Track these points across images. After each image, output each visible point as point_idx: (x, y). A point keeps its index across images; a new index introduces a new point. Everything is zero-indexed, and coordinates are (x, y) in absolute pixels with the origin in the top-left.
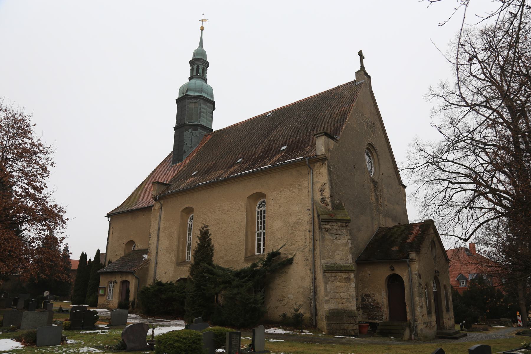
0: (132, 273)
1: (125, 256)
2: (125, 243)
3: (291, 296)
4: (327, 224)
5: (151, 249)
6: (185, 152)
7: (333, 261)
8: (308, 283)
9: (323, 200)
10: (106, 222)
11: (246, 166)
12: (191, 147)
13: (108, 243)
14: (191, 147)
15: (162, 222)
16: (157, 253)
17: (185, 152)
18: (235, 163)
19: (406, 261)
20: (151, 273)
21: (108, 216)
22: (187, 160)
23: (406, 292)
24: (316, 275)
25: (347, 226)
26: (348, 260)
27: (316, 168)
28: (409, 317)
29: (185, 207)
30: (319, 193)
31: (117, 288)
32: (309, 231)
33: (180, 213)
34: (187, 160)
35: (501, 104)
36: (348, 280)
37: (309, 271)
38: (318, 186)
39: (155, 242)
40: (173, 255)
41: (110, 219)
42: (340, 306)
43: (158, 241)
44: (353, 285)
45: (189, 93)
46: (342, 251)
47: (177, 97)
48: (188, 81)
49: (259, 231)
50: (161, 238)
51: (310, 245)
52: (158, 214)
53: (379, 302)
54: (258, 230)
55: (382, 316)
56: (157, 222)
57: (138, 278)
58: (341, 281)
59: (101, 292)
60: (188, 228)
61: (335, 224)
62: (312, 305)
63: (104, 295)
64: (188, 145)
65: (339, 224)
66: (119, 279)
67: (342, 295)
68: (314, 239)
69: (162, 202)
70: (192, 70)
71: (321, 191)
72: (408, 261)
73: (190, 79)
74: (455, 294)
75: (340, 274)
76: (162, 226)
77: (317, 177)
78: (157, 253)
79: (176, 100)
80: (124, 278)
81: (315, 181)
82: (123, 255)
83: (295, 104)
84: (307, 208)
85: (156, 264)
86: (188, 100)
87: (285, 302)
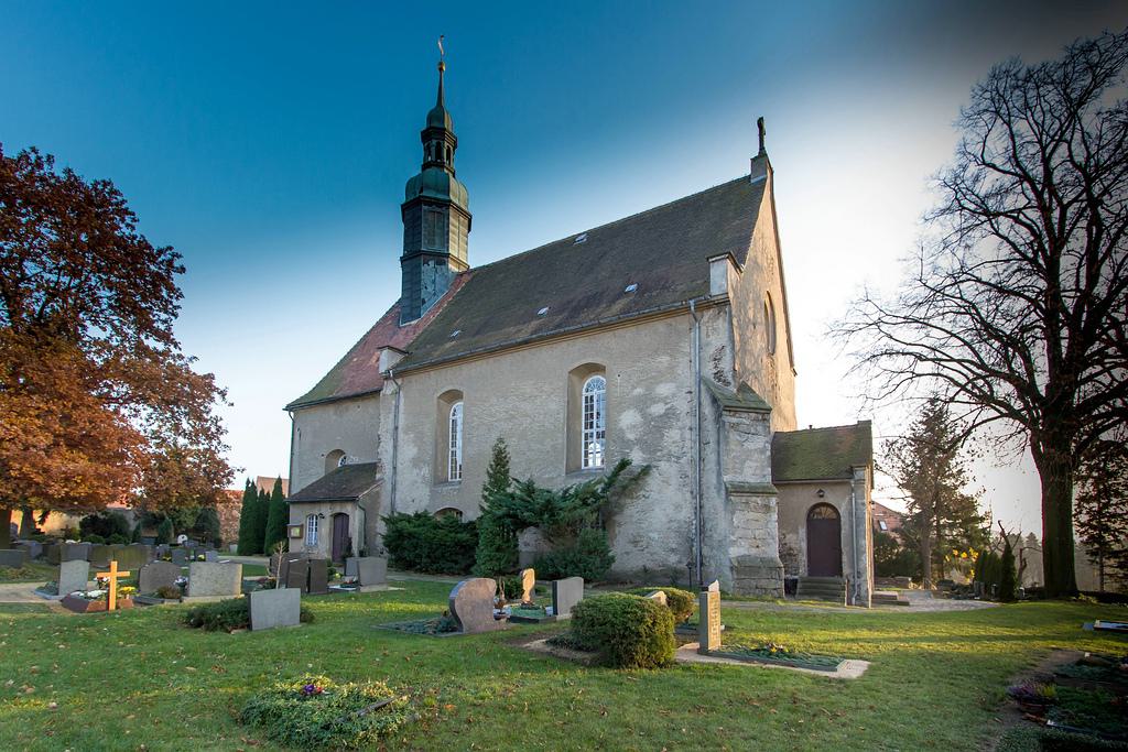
0: (353, 500)
1: (325, 477)
2: (326, 454)
3: (655, 535)
4: (734, 416)
5: (384, 461)
6: (424, 302)
7: (739, 478)
8: (686, 513)
9: (719, 375)
10: (286, 420)
11: (558, 319)
12: (435, 294)
13: (292, 454)
14: (435, 294)
15: (401, 416)
16: (395, 468)
17: (424, 302)
18: (623, 294)
19: (850, 484)
20: (385, 501)
21: (289, 408)
22: (429, 315)
23: (843, 532)
24: (704, 501)
25: (765, 420)
26: (764, 476)
27: (705, 319)
28: (846, 570)
29: (446, 389)
30: (712, 364)
31: (325, 527)
32: (691, 429)
33: (435, 401)
34: (429, 315)
35: (1080, 195)
36: (767, 508)
37: (688, 495)
38: (711, 351)
39: (391, 450)
40: (426, 471)
41: (292, 414)
42: (754, 551)
43: (395, 447)
44: (775, 517)
45: (424, 194)
46: (756, 461)
47: (404, 200)
48: (420, 171)
49: (589, 431)
50: (400, 442)
51: (692, 453)
52: (394, 402)
53: (793, 546)
54: (586, 428)
55: (798, 568)
56: (392, 416)
57: (364, 509)
58: (756, 509)
59: (295, 532)
60: (584, 405)
61: (746, 415)
62: (694, 549)
63: (300, 537)
64: (430, 289)
65: (753, 415)
66: (327, 510)
67: (757, 532)
68: (702, 443)
69: (399, 381)
70: (427, 150)
71: (715, 359)
72: (852, 482)
73: (426, 166)
74: (880, 540)
75: (754, 498)
76: (401, 423)
77: (708, 336)
78: (395, 468)
79: (402, 206)
80: (338, 509)
81: (703, 341)
82: (324, 475)
83: (676, 202)
84: (689, 389)
85: (394, 489)
86: (425, 207)
87: (644, 544)
